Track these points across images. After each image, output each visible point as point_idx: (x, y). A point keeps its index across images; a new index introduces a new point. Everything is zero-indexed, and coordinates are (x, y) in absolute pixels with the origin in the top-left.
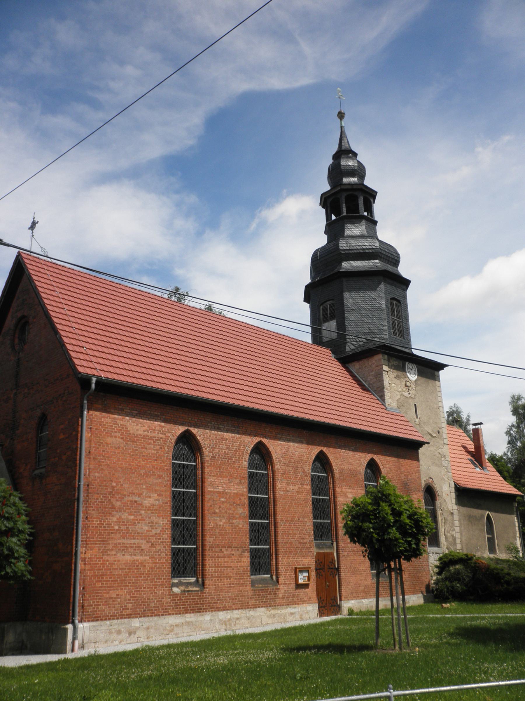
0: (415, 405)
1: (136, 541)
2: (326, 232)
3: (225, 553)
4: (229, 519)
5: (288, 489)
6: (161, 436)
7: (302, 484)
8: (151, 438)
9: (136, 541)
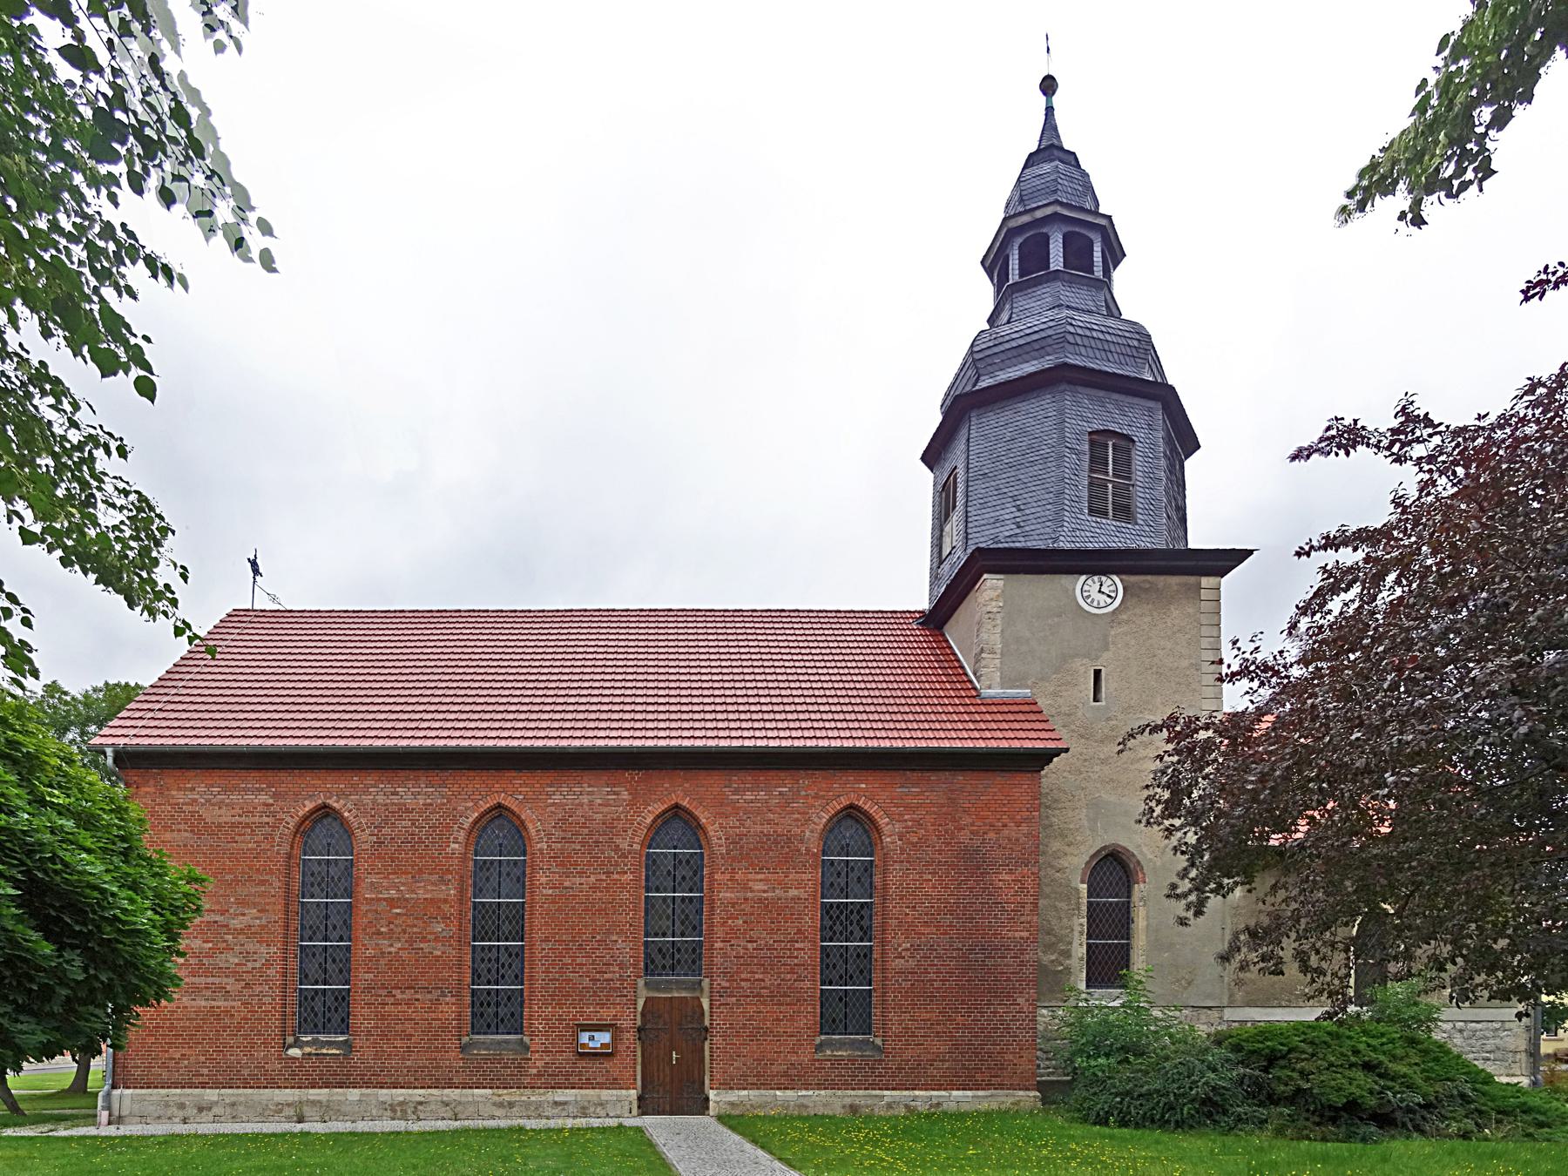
0: (1097, 673)
1: (217, 980)
2: (1172, 388)
3: (399, 996)
4: (411, 941)
5: (567, 884)
6: (266, 819)
7: (608, 873)
8: (247, 825)
9: (217, 980)
